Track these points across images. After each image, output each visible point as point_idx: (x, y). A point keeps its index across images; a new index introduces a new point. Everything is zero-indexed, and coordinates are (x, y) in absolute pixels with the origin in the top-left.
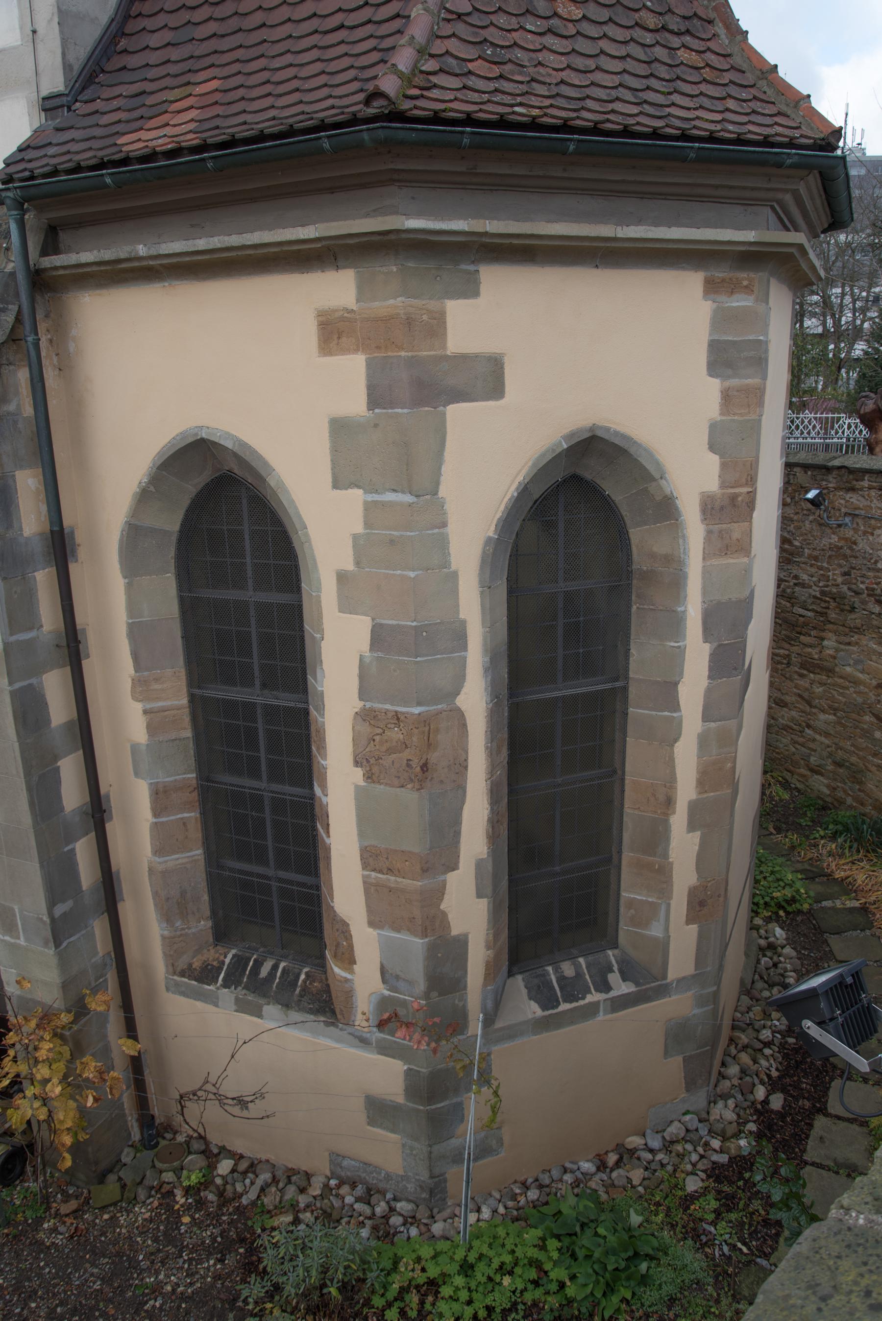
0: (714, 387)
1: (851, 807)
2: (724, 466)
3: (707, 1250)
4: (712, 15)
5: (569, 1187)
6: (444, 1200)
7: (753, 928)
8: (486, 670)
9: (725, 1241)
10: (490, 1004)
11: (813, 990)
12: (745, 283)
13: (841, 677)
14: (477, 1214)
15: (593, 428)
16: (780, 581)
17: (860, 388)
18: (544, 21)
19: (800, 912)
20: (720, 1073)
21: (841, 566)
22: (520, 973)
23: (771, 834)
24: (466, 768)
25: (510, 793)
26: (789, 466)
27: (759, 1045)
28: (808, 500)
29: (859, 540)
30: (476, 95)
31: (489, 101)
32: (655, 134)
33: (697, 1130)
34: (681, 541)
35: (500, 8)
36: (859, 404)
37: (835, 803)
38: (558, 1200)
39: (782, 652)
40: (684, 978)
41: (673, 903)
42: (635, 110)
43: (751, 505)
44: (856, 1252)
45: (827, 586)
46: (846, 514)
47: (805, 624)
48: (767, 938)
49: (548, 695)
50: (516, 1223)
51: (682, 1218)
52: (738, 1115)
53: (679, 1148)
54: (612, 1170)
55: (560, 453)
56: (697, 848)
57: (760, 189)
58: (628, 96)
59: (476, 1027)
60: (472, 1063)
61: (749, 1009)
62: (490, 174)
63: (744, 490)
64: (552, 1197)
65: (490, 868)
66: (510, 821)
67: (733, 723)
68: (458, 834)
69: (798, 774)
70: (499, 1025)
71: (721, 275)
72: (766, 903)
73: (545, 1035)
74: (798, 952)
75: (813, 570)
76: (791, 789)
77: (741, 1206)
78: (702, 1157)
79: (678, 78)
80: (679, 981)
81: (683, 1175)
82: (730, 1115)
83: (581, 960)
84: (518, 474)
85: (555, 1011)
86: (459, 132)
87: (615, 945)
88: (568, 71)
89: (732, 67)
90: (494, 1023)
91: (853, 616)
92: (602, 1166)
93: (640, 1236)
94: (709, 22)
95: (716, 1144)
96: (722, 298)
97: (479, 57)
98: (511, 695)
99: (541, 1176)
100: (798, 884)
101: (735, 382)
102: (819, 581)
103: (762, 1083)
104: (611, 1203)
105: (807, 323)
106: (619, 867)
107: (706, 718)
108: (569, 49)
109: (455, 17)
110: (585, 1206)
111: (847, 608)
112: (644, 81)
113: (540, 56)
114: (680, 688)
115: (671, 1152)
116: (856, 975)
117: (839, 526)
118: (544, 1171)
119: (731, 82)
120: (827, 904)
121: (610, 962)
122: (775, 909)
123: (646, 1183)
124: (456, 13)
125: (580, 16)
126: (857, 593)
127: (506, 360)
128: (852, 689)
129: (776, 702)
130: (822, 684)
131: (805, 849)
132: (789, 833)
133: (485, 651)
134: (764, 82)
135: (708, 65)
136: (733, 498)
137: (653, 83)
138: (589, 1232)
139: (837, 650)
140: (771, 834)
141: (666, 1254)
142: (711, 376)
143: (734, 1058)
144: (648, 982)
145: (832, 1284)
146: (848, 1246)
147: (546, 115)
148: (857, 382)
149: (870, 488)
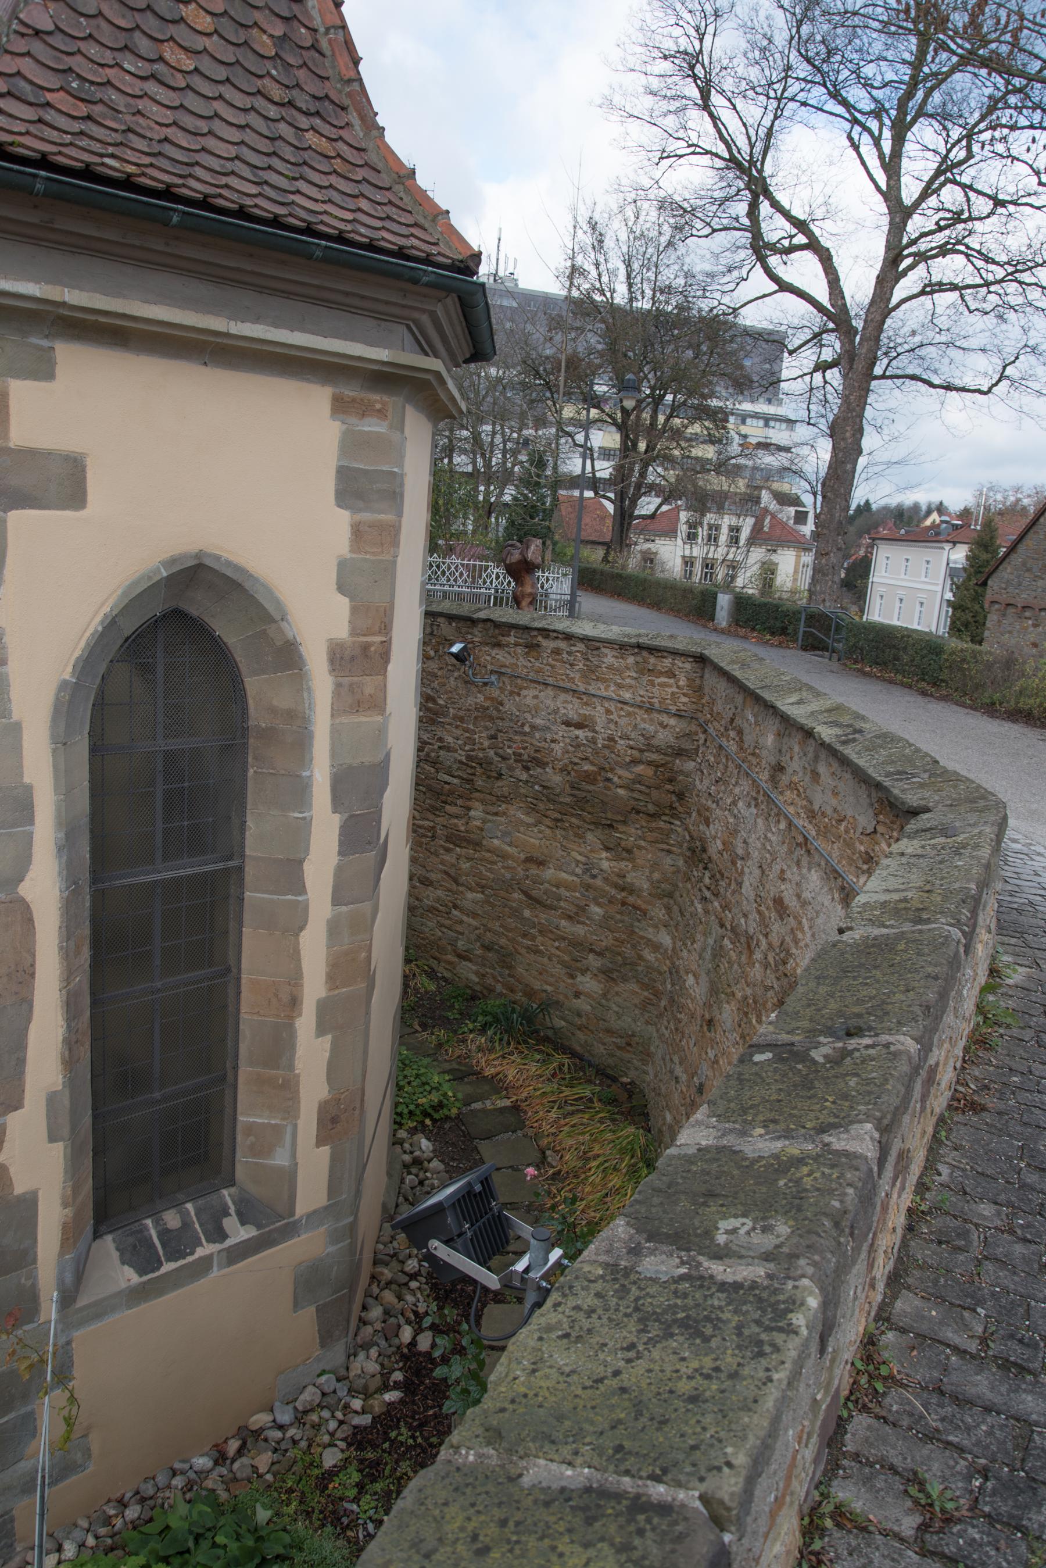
0: (342, 520)
1: (501, 995)
2: (354, 610)
3: (350, 1533)
4: (346, 102)
5: (179, 1494)
6: (11, 1545)
7: (396, 1142)
8: (60, 849)
9: (370, 1518)
10: (69, 1277)
11: (440, 1204)
12: (378, 406)
13: (489, 851)
14: (57, 1555)
15: (199, 555)
16: (421, 746)
17: (509, 536)
18: (147, 64)
19: (447, 1118)
20: (360, 1319)
21: (487, 728)
22: (110, 1232)
23: (416, 1031)
24: (33, 975)
25: (94, 1004)
26: (428, 614)
27: (404, 1279)
28: (452, 654)
29: (506, 701)
30: (55, 133)
31: (71, 144)
32: (276, 222)
33: (334, 1392)
34: (305, 695)
35: (90, 36)
36: (505, 551)
37: (485, 992)
38: (166, 1513)
39: (426, 823)
40: (315, 1212)
41: (300, 1123)
42: (254, 190)
43: (385, 656)
44: (464, 1494)
45: (473, 750)
46: (492, 672)
47: (451, 793)
48: (412, 1153)
49: (143, 879)
50: (110, 1555)
51: (319, 1502)
52: (382, 1365)
53: (314, 1417)
54: (233, 1461)
55: (158, 582)
56: (328, 1054)
57: (395, 304)
58: (246, 172)
59: (50, 1311)
60: (43, 1361)
61: (393, 1238)
62: (71, 233)
63: (378, 639)
64: (158, 1509)
65: (67, 1102)
66: (94, 1040)
67: (366, 907)
68: (22, 1062)
69: (446, 961)
70: (82, 1302)
71: (351, 394)
72: (410, 1112)
73: (143, 1306)
74: (446, 1164)
75: (459, 732)
76: (437, 979)
77: (387, 1472)
78: (341, 1423)
79: (305, 163)
80: (309, 1216)
81: (320, 1449)
82: (372, 1367)
83: (189, 1206)
84: (103, 604)
85: (156, 1274)
86: (30, 174)
87: (231, 1182)
88: (174, 129)
89: (366, 164)
90: (75, 1301)
91: (500, 783)
92: (221, 1458)
93: (269, 1534)
94: (343, 109)
95: (357, 1404)
96: (353, 420)
97: (62, 88)
98: (95, 880)
99: (143, 1487)
100: (446, 1087)
102: (465, 744)
103: (409, 1322)
104: (232, 1502)
105: (457, 459)
106: (235, 1087)
107: (336, 901)
108: (177, 104)
109: (30, 32)
110: (200, 1513)
111: (494, 774)
112: (266, 159)
113: (141, 104)
114: (306, 866)
115: (304, 1424)
116: (486, 1182)
117: (485, 684)
118: (146, 1480)
119: (364, 179)
120: (475, 1106)
121: (226, 1204)
122: (420, 1118)
123: (275, 1468)
124: (34, 29)
125: (192, 68)
126: (504, 758)
127: (89, 462)
128: (500, 864)
129: (419, 880)
130: (469, 859)
131: (453, 1046)
132: (436, 1030)
133: (59, 824)
134: (400, 188)
135: (339, 155)
136: (365, 648)
137: (276, 162)
138: (205, 1544)
139: (484, 822)
140: (416, 1031)
141: (301, 1550)
142: (339, 506)
143: (376, 1298)
144: (272, 1221)
145: (438, 1536)
146: (456, 1490)
147: (144, 174)
148: (506, 528)
149: (516, 645)
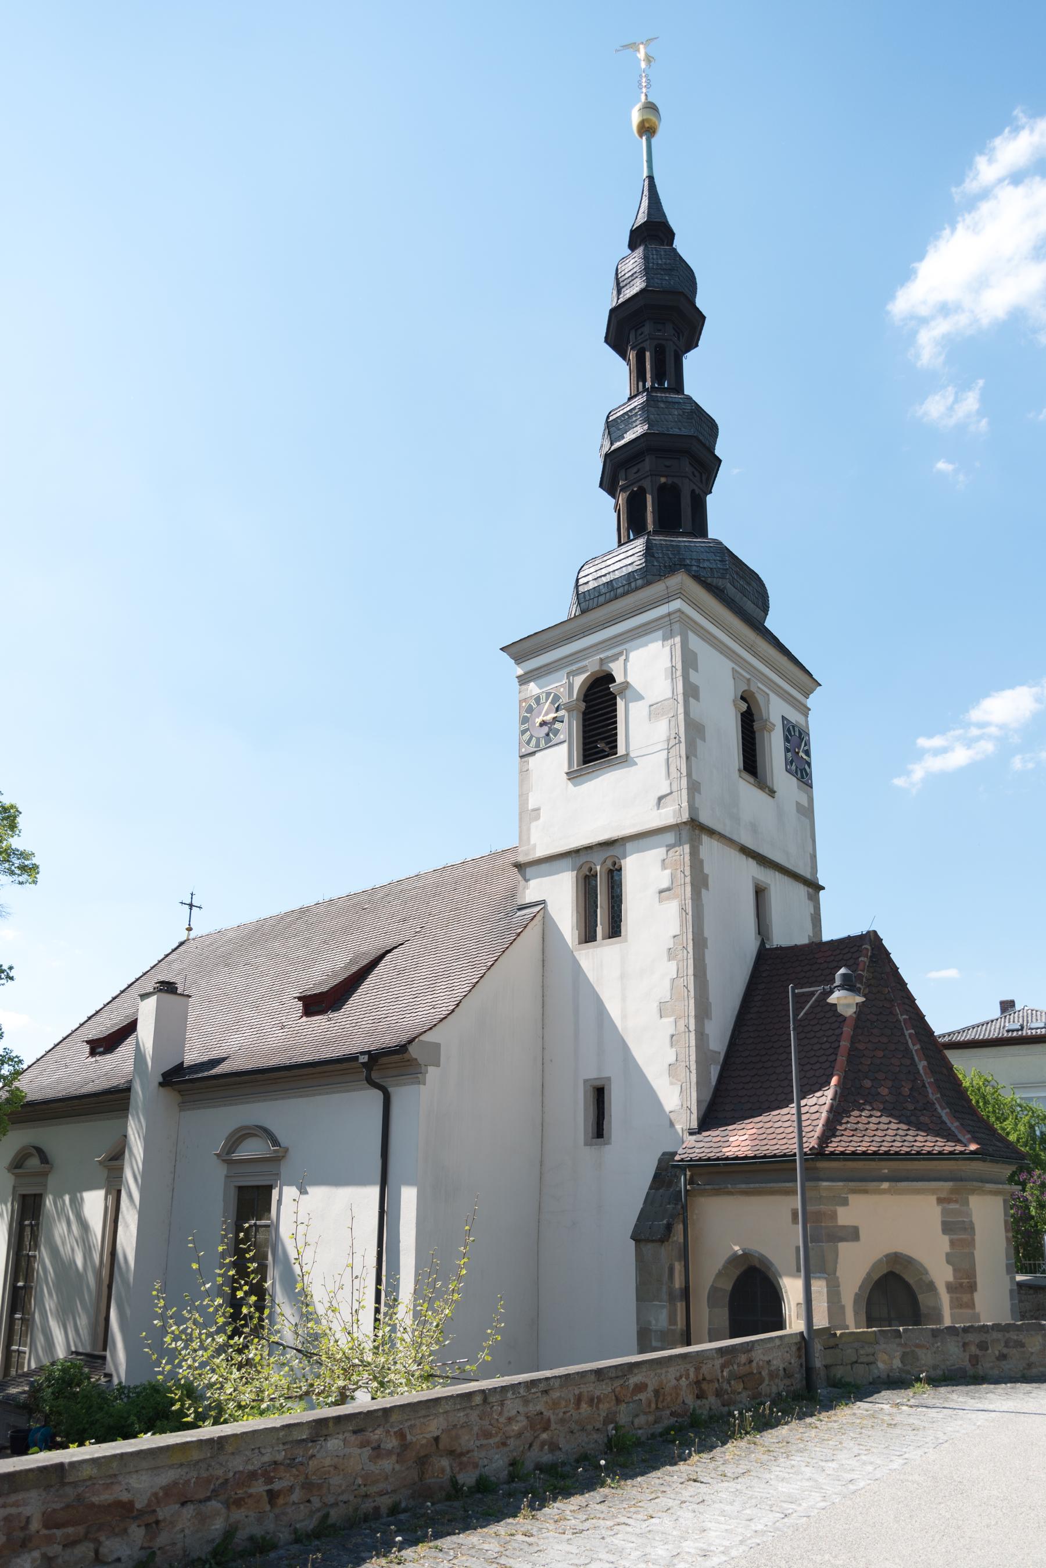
2: (955, 1270)
49: (649, 508)
96: (945, 1205)
101: (955, 1237)
